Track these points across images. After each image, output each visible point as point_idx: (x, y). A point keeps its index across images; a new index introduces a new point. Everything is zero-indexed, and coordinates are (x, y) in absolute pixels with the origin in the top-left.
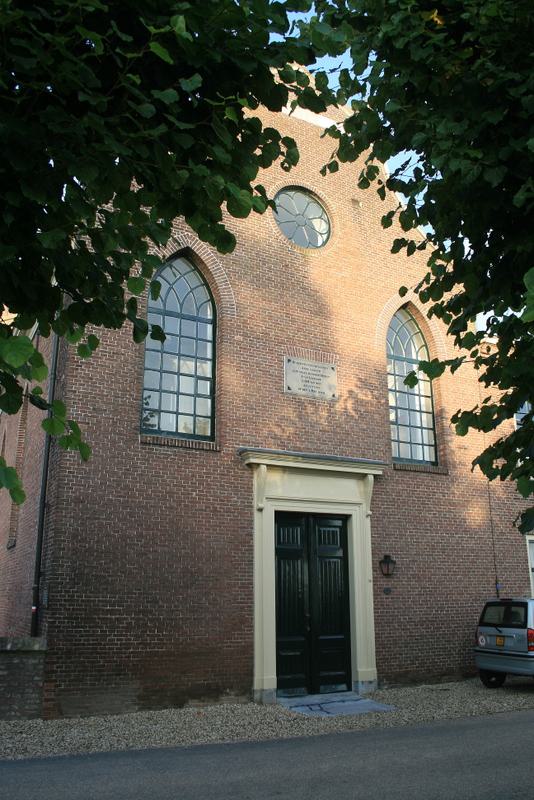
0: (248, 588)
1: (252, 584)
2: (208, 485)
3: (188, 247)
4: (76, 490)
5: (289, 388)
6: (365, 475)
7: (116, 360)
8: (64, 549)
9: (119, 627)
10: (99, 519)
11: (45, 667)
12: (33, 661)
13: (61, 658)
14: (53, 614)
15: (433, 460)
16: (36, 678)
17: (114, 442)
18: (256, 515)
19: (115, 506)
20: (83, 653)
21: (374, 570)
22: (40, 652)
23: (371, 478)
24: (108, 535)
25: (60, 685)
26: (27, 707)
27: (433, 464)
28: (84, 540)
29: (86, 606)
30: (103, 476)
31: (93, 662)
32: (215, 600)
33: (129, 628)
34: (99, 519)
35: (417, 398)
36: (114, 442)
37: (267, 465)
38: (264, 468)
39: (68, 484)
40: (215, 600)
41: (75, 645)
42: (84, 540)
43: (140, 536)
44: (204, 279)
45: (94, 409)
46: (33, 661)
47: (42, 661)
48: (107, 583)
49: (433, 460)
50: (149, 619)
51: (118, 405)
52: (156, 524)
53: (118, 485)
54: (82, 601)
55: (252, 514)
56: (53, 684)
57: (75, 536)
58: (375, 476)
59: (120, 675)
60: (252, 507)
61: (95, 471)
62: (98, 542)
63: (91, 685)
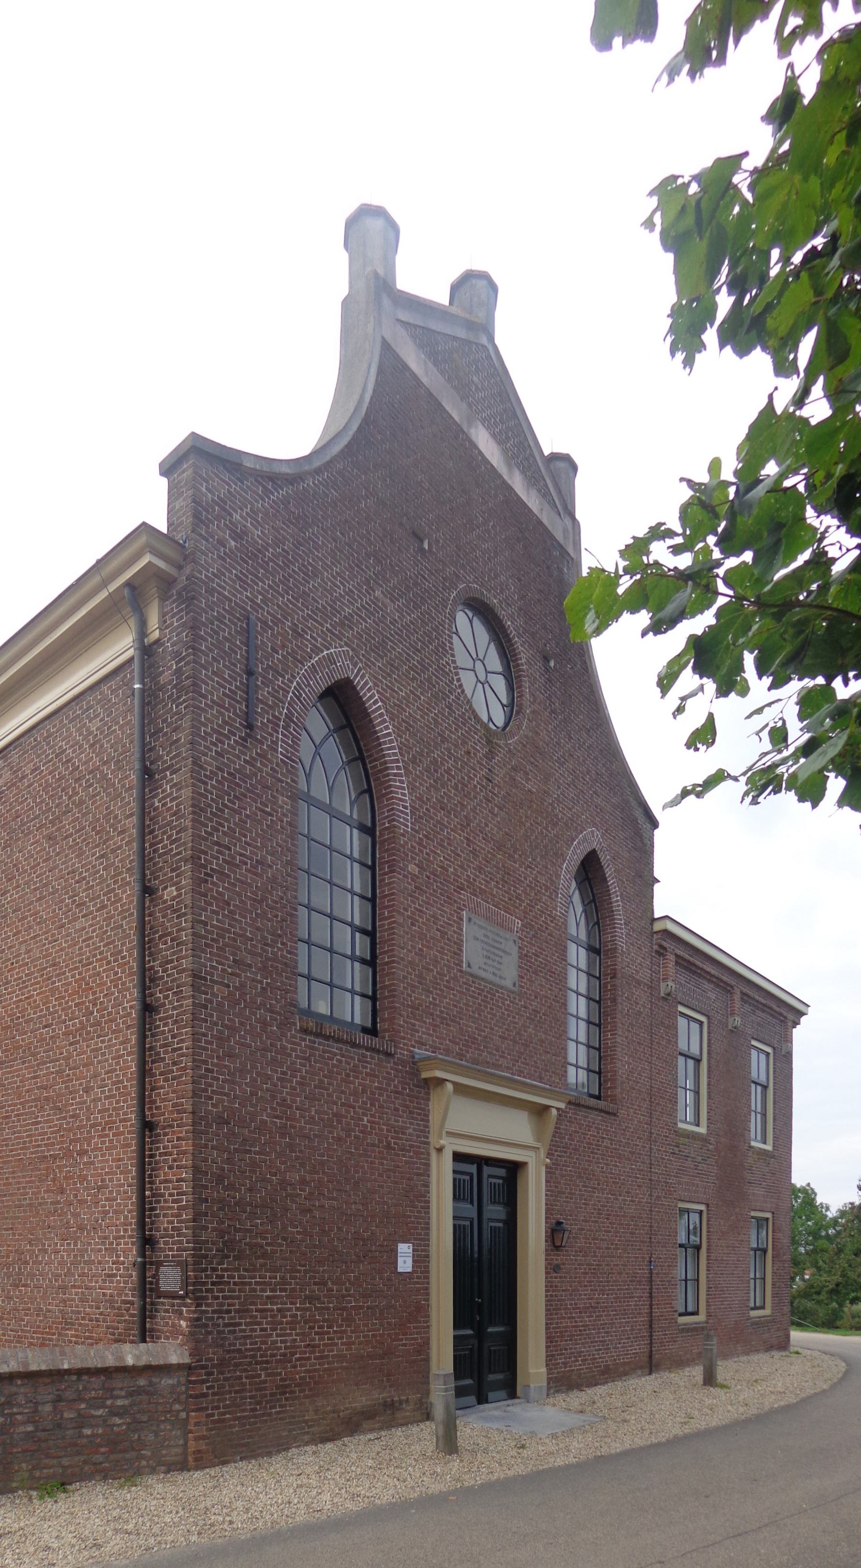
0: (425, 1262)
1: (428, 1256)
2: (381, 1107)
3: (348, 678)
4: (218, 1101)
5: (469, 966)
6: (547, 1108)
7: (261, 876)
8: (206, 1201)
9: (281, 1323)
10: (249, 1152)
11: (187, 1389)
12: (170, 1382)
13: (212, 1374)
14: (199, 1305)
15: (369, 1024)
16: (177, 1407)
17: (264, 1024)
18: (434, 1155)
19: (271, 1132)
20: (240, 1364)
21: (546, 1241)
22: (180, 1367)
23: (554, 1112)
24: (264, 1180)
25: (213, 1415)
26: (164, 1452)
27: (365, 1030)
28: (231, 1187)
29: (240, 1291)
30: (254, 1080)
31: (253, 1377)
32: (389, 1280)
33: (293, 1324)
34: (249, 1152)
35: (357, 922)
36: (264, 1024)
37: (455, 1084)
38: (450, 1086)
39: (206, 1090)
40: (389, 1280)
41: (229, 1352)
42: (231, 1187)
43: (303, 1182)
44: (360, 750)
45: (235, 961)
46: (170, 1382)
47: (183, 1380)
48: (264, 1255)
49: (369, 1024)
50: (317, 1309)
51: (268, 959)
52: (322, 1163)
53: (274, 1097)
54: (235, 1284)
55: (429, 1154)
56: (204, 1414)
57: (220, 1179)
58: (558, 1109)
59: (285, 1393)
60: (428, 1143)
61: (242, 1071)
62: (250, 1190)
63: (252, 1410)
